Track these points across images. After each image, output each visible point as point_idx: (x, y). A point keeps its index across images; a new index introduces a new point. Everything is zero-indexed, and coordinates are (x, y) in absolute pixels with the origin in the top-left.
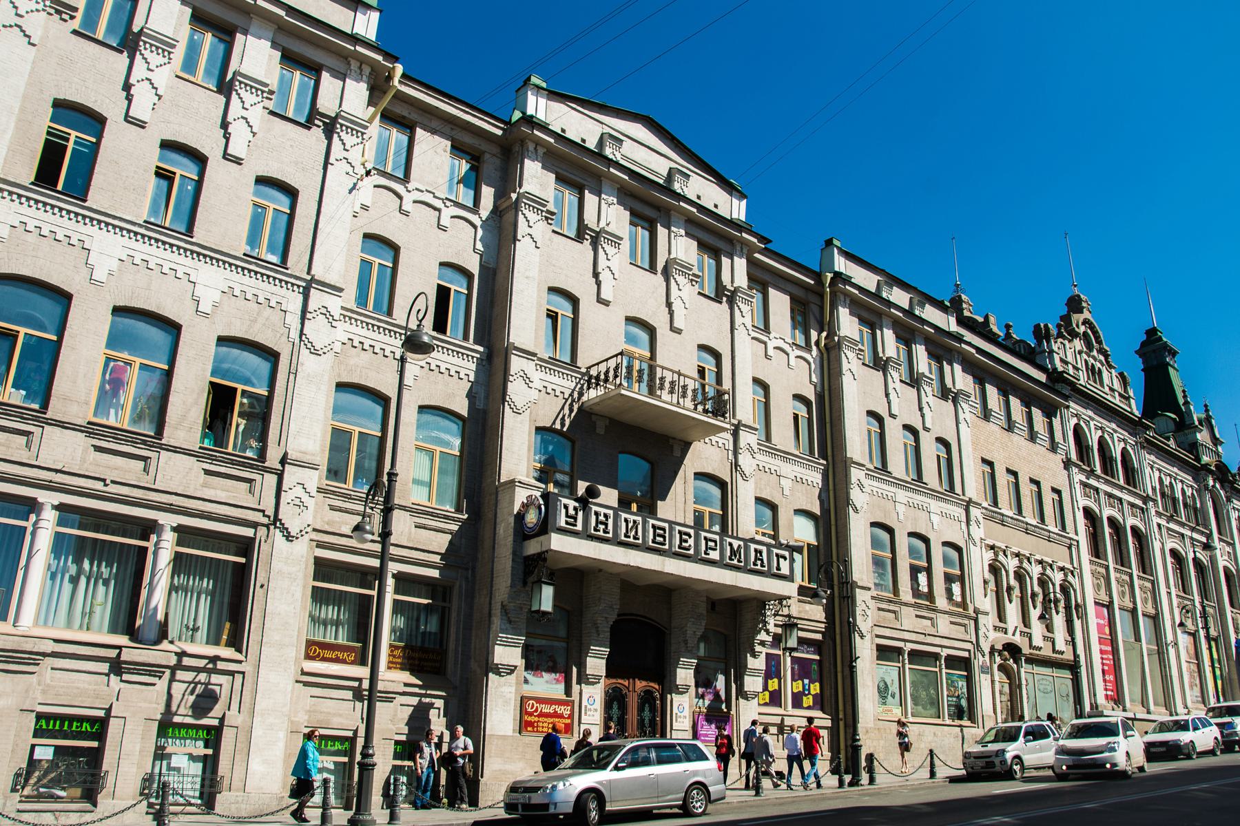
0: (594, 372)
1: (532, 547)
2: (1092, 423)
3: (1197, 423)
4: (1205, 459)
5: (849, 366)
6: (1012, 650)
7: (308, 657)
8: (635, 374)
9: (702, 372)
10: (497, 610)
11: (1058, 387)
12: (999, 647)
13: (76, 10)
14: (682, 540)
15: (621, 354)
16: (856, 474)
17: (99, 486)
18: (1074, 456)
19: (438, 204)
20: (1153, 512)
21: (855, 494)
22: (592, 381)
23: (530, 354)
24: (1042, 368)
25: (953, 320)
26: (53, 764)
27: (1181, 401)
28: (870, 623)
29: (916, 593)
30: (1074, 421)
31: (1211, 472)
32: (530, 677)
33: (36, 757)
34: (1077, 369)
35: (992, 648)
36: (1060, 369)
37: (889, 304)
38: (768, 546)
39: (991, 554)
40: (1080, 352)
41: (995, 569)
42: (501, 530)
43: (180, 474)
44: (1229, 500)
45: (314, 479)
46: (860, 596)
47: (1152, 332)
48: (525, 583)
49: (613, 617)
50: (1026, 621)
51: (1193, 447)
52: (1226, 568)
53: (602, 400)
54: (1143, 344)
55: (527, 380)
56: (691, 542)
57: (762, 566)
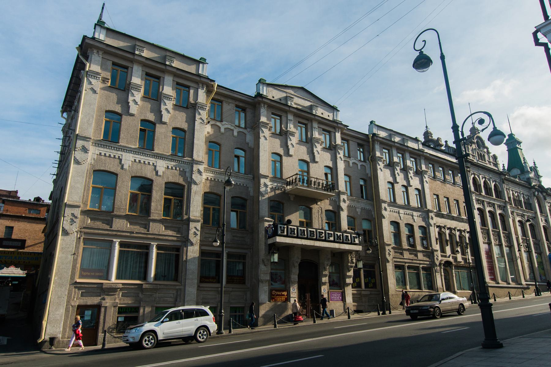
0: (288, 180)
1: (270, 241)
2: (480, 176)
3: (529, 170)
6: (448, 264)
8: (301, 180)
9: (326, 174)
10: (261, 261)
12: (443, 262)
13: (109, 79)
14: (320, 235)
15: (297, 174)
17: (129, 234)
19: (232, 128)
21: (384, 212)
22: (288, 184)
26: (124, 322)
27: (523, 162)
28: (391, 257)
29: (410, 245)
30: (473, 176)
32: (273, 283)
33: (119, 320)
34: (474, 156)
35: (440, 264)
37: (394, 142)
38: (351, 234)
39: (437, 230)
40: (475, 149)
41: (440, 234)
42: (260, 236)
44: (545, 199)
46: (387, 248)
48: (269, 253)
49: (299, 261)
51: (529, 180)
52: (544, 226)
53: (292, 190)
56: (323, 235)
57: (281, 227)
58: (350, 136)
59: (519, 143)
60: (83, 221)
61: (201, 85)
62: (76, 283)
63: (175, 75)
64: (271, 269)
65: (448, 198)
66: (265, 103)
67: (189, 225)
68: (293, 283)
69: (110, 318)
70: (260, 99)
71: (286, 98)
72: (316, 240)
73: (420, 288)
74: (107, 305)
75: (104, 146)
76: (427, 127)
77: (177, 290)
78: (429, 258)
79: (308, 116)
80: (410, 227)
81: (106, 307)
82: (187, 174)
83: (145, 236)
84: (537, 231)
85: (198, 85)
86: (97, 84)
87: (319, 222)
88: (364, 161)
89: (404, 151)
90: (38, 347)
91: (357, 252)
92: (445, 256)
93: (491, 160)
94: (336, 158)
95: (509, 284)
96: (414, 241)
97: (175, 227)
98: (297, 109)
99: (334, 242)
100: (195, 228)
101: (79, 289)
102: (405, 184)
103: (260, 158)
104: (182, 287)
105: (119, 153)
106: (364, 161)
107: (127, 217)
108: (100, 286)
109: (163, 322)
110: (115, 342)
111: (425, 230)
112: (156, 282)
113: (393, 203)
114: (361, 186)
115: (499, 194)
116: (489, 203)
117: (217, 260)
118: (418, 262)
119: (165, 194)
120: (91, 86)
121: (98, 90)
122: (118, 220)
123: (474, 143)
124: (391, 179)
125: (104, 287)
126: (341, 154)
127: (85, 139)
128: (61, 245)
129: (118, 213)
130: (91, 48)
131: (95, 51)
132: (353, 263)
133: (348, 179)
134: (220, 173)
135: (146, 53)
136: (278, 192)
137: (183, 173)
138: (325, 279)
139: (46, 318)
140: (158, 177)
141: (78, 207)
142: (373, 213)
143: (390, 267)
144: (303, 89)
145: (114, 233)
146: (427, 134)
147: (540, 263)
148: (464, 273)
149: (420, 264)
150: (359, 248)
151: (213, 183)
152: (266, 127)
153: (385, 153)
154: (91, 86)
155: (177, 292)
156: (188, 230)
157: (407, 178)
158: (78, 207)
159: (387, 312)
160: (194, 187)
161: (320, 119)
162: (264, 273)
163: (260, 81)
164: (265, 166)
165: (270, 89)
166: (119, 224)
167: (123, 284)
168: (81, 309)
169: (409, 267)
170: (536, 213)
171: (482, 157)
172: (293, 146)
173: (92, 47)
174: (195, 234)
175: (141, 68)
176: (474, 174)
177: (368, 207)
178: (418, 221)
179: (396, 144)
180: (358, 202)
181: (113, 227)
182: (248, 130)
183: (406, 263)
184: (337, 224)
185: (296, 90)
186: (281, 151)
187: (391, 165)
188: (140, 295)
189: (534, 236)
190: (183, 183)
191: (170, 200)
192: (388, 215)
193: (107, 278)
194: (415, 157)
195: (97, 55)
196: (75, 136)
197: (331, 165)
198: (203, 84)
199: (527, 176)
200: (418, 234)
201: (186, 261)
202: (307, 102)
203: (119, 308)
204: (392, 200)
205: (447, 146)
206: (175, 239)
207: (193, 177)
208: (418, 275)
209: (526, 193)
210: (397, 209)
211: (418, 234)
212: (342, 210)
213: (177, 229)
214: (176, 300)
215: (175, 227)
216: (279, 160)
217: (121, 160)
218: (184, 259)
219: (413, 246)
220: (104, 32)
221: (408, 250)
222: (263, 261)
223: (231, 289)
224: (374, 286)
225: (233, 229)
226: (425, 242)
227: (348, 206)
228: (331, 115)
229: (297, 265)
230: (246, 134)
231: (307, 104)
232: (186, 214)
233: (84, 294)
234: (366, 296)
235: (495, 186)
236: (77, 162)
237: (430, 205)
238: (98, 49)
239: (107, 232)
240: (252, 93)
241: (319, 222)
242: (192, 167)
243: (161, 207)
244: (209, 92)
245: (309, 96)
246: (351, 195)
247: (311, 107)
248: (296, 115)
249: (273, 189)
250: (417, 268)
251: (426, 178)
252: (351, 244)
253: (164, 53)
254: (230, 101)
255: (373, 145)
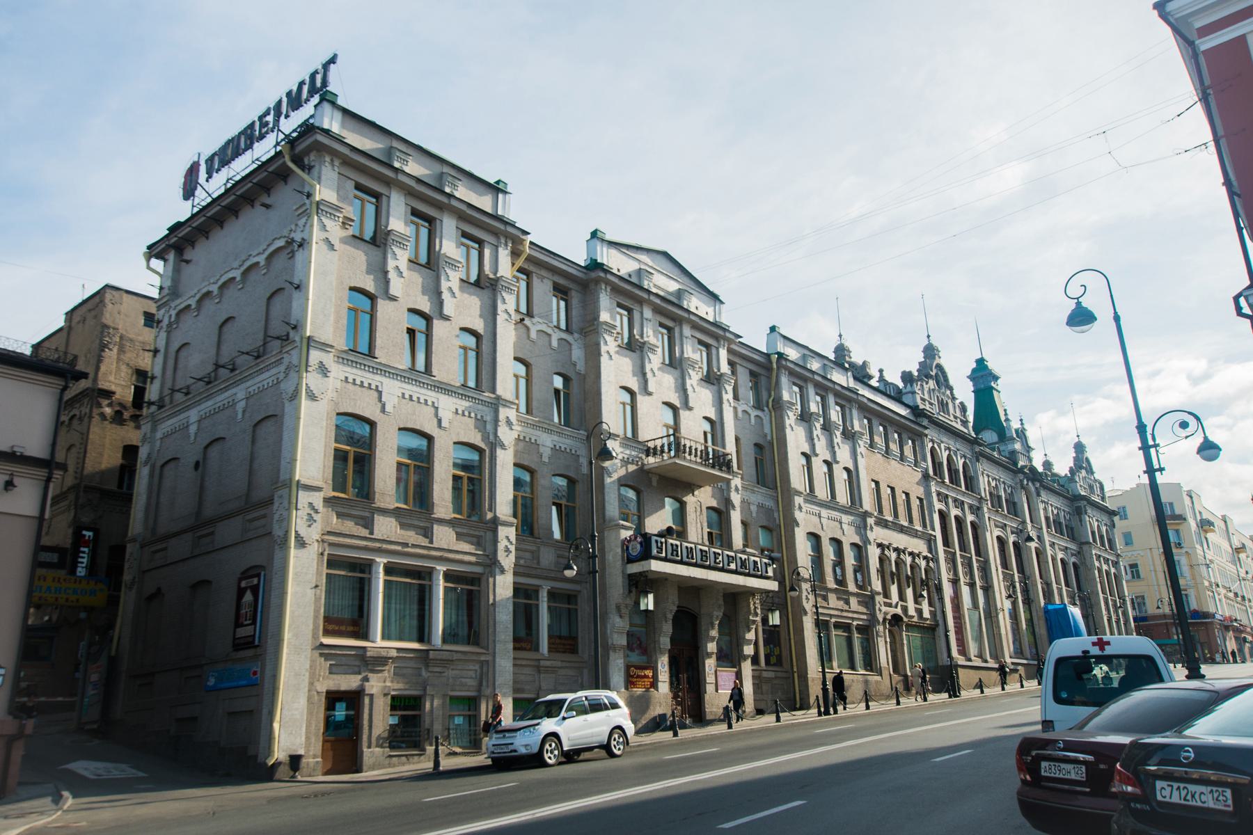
0: (651, 445)
1: (634, 568)
4: (1021, 464)
5: (449, 284)
7: (327, 633)
11: (919, 420)
12: (889, 617)
16: (798, 500)
17: (399, 548)
18: (931, 472)
19: (549, 331)
20: (985, 510)
21: (799, 515)
23: (324, 347)
24: (907, 406)
25: (851, 380)
27: (1003, 418)
29: (838, 582)
30: (930, 445)
31: (1024, 473)
35: (885, 619)
36: (921, 407)
41: (882, 560)
43: (386, 527)
45: (317, 499)
47: (981, 362)
50: (902, 597)
51: (1013, 455)
54: (974, 371)
55: (323, 370)
58: (538, 264)
59: (996, 378)
60: (327, 521)
61: (503, 241)
62: (322, 645)
63: (461, 217)
64: (631, 625)
65: (877, 483)
66: (608, 283)
67: (495, 531)
68: (662, 653)
69: (380, 719)
70: (602, 275)
71: (639, 272)
72: (709, 568)
73: (853, 667)
74: (374, 691)
75: (353, 364)
76: (840, 336)
77: (482, 662)
78: (867, 608)
79: (675, 315)
80: (837, 543)
81: (371, 696)
82: (488, 426)
83: (425, 552)
84: (1024, 557)
85: (498, 238)
86: (335, 230)
87: (697, 531)
88: (568, 330)
89: (826, 389)
90: (267, 774)
91: (767, 592)
92: (890, 605)
93: (958, 414)
94: (494, 314)
95: (986, 661)
96: (844, 574)
97: (473, 536)
98: (657, 295)
99: (735, 572)
100: (507, 538)
101: (327, 657)
102: (425, 305)
103: (603, 397)
104: (489, 658)
105: (378, 378)
106: (568, 330)
107: (396, 513)
108: (360, 652)
109: (564, 718)
110: (390, 766)
111: (859, 550)
112: (446, 647)
113: (811, 496)
114: (557, 392)
115: (971, 484)
116: (955, 500)
117: (526, 605)
118: (850, 615)
119: (336, 441)
120: (324, 235)
121: (337, 245)
122: (381, 518)
123: (931, 377)
124: (807, 449)
125: (369, 654)
126: (508, 303)
127: (324, 347)
128: (295, 567)
129: (382, 505)
130: (318, 151)
131: (328, 159)
132: (756, 614)
133: (522, 370)
134: (534, 426)
135: (414, 167)
136: (632, 468)
137: (481, 424)
138: (712, 647)
139: (277, 717)
140: (442, 432)
141: (318, 489)
142: (776, 515)
143: (808, 623)
144: (665, 255)
145: (378, 545)
146: (841, 350)
147: (1030, 622)
148: (916, 635)
149: (853, 619)
150: (773, 586)
151: (521, 444)
152: (332, 216)
153: (621, 315)
154: (324, 235)
155: (481, 668)
156: (495, 541)
157: (831, 446)
158: (318, 489)
159: (840, 708)
160: (499, 452)
161: (463, 207)
162: (618, 629)
163: (594, 234)
164: (612, 416)
165: (613, 252)
166: (386, 527)
167: (399, 650)
168: (333, 698)
169: (837, 626)
170: (1024, 522)
171: (943, 406)
172: (400, 274)
173: (320, 148)
174: (507, 550)
175: (402, 198)
176: (932, 441)
177: (769, 503)
178: (850, 536)
179: (652, 298)
180: (753, 492)
181: (376, 531)
182: (576, 335)
183: (831, 616)
184: (724, 537)
185: (655, 255)
186: (634, 384)
187: (634, 346)
188: (424, 673)
189: (1021, 569)
190: (482, 445)
191: (346, 452)
192: (806, 519)
193: (365, 636)
194: (843, 403)
195: (329, 167)
196: (305, 341)
197: (713, 416)
198: (508, 236)
199: (1010, 447)
200: (850, 560)
201: (494, 604)
202: (672, 282)
203: (393, 698)
204: (629, 435)
205: (881, 379)
206: (473, 559)
207: (499, 434)
208: (849, 641)
209: (1009, 482)
210: (816, 509)
211: (850, 560)
212: (734, 507)
213: (475, 540)
214: (480, 684)
215: (473, 536)
216: (368, 308)
217: (380, 393)
218: (491, 601)
219: (841, 582)
220: (338, 115)
221: (835, 591)
222: (618, 608)
223: (559, 664)
224: (779, 662)
225: (557, 541)
226: (838, 570)
227: (518, 439)
228: (711, 310)
229: (670, 616)
230: (570, 344)
231: (673, 286)
232: (490, 510)
233: (334, 669)
234: (769, 680)
235: (965, 464)
236: (312, 397)
237: (868, 504)
238: (334, 153)
239: (364, 543)
240: (580, 257)
241: (697, 531)
242: (496, 412)
243: (448, 494)
244: (515, 254)
245: (677, 271)
246: (529, 411)
247: (679, 294)
248: (657, 310)
249: (626, 462)
250: (846, 627)
251: (862, 448)
252: (761, 577)
253: (438, 168)
254: (544, 273)
255: (778, 377)
